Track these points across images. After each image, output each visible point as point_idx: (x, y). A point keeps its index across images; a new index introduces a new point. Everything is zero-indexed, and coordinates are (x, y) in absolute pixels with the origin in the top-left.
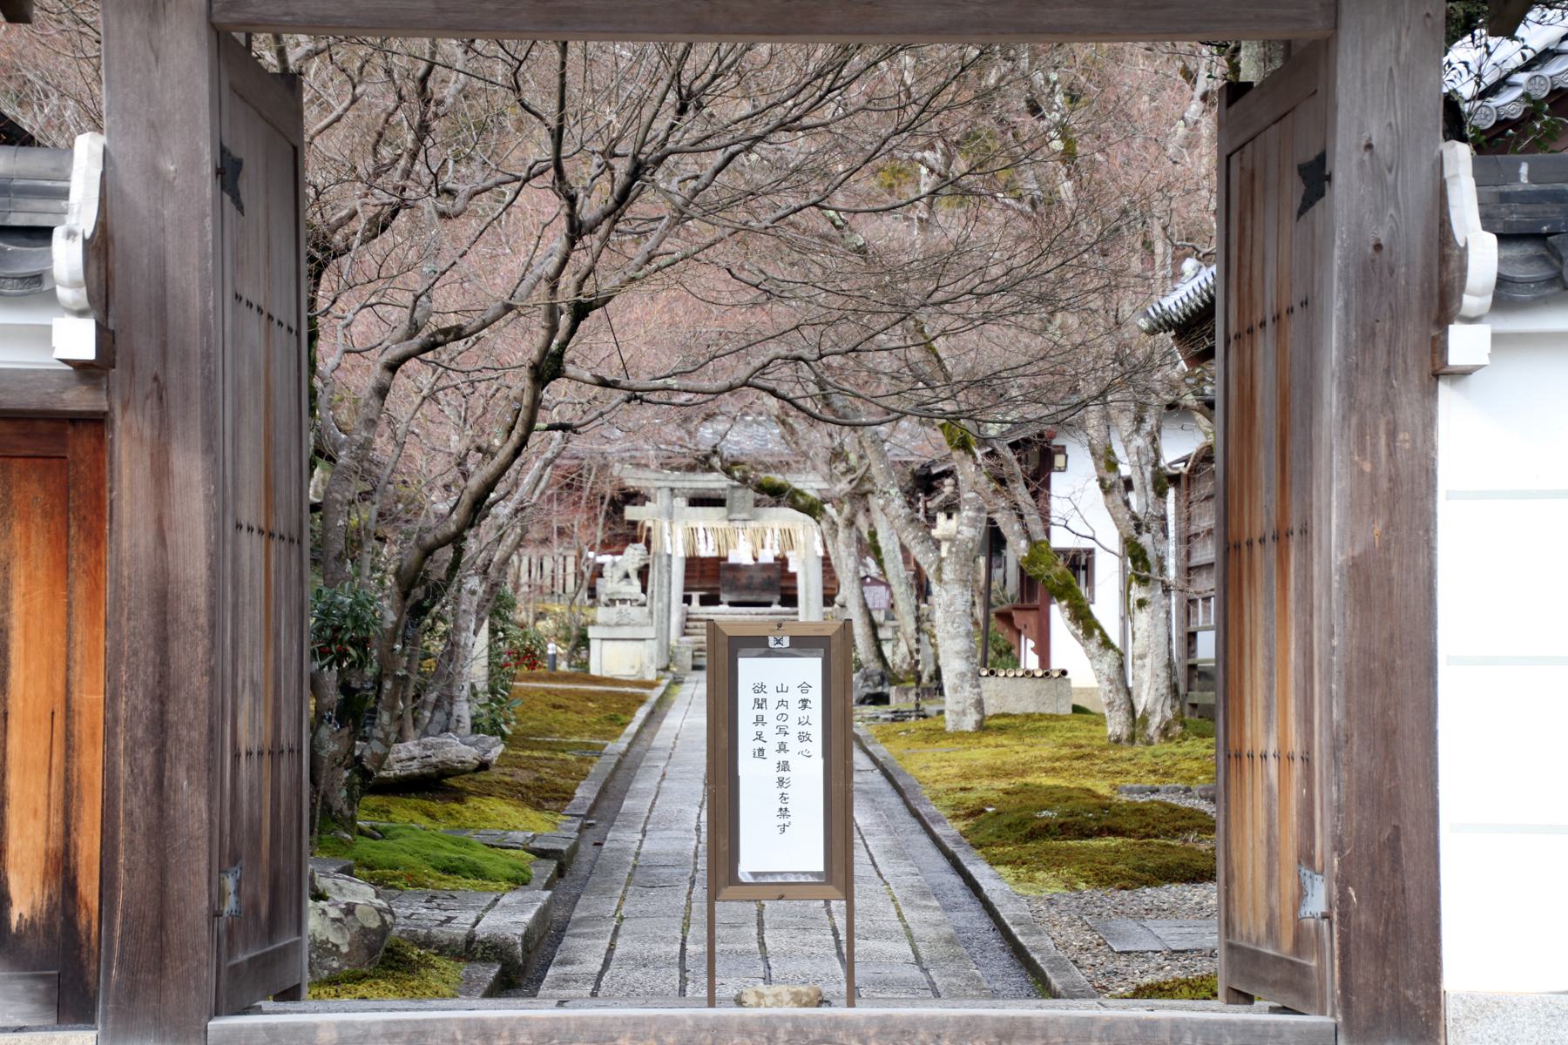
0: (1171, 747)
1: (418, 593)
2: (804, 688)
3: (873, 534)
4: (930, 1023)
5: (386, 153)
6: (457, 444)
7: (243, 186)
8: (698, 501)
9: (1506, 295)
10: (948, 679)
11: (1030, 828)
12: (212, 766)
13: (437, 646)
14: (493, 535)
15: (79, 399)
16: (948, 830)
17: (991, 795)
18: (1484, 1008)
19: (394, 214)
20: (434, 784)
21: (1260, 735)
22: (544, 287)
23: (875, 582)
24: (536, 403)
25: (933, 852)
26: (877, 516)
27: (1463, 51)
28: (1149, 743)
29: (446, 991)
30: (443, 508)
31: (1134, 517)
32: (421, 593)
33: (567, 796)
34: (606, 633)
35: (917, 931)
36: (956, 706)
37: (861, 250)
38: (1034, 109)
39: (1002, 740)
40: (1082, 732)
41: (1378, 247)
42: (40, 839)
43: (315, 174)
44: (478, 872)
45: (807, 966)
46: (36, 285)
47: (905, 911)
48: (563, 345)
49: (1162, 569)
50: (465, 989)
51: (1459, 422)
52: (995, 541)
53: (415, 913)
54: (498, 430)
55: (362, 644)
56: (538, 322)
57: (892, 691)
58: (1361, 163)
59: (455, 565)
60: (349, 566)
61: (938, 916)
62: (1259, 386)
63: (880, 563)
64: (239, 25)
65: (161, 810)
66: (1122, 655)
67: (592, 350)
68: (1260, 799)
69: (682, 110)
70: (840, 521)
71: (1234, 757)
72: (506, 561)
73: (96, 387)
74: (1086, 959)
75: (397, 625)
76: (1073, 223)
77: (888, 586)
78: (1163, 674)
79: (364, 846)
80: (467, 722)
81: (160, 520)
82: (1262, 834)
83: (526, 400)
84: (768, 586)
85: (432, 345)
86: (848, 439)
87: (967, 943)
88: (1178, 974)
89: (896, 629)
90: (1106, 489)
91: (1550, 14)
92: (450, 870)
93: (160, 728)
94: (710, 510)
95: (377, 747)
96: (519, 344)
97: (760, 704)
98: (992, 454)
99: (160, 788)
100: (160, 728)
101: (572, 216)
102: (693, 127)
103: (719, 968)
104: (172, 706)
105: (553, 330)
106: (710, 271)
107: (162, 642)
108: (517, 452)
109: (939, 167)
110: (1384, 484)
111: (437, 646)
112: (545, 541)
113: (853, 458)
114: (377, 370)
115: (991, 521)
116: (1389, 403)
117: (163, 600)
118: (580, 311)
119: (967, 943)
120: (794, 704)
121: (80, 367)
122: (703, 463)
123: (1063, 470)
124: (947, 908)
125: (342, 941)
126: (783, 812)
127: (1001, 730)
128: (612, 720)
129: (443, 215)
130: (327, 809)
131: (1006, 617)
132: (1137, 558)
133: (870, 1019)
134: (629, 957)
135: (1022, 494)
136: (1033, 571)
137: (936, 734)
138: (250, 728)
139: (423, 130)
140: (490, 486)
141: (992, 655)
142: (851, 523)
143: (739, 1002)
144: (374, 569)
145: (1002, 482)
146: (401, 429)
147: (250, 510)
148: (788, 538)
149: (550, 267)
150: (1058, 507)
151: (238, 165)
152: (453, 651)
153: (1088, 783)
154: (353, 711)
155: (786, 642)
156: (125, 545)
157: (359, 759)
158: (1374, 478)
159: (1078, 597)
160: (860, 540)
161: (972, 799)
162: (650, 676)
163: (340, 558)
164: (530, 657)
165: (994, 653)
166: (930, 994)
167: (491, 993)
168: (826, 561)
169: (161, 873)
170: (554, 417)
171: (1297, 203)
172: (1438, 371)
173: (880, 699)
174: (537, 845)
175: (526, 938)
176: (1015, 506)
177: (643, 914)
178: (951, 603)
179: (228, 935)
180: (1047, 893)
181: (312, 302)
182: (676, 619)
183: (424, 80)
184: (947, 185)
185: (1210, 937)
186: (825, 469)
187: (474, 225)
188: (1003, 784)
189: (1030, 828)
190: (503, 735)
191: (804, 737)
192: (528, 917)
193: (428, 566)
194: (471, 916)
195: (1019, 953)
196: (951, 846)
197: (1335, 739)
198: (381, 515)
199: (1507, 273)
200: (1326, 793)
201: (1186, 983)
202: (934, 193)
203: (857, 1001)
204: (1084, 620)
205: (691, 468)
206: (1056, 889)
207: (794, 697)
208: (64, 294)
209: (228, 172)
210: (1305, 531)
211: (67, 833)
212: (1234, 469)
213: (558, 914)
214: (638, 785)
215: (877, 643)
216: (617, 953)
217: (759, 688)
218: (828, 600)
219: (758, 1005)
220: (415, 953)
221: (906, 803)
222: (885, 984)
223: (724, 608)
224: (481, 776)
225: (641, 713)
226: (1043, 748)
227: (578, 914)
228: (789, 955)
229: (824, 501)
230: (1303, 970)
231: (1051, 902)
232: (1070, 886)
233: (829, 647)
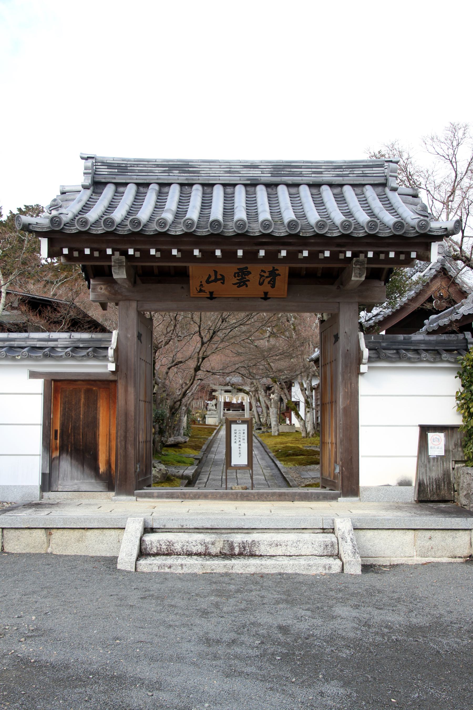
0: (313, 439)
1: (173, 410)
2: (244, 430)
3: (259, 398)
4: (266, 493)
5: (169, 330)
6: (181, 382)
7: (142, 339)
8: (226, 391)
9: (370, 360)
10: (272, 425)
11: (287, 454)
12: (135, 445)
13: (177, 419)
14: (187, 399)
15: (112, 378)
16: (272, 455)
17: (280, 448)
18: (367, 489)
19: (170, 341)
20: (176, 445)
21: (328, 440)
22: (197, 354)
23: (259, 407)
24: (195, 375)
25: (269, 459)
26: (259, 394)
27: (363, 314)
28: (310, 438)
29: (178, 485)
30: (178, 393)
31: (307, 396)
32: (174, 410)
33: (201, 448)
34: (209, 416)
35: (266, 474)
36: (274, 430)
37: (256, 346)
38: (288, 321)
39: (282, 437)
40: (297, 436)
41: (348, 350)
42: (105, 457)
43: (155, 334)
44: (184, 462)
45: (245, 481)
46: (105, 358)
47: (264, 471)
48: (200, 364)
49: (312, 405)
50: (181, 484)
51: (362, 382)
52: (281, 400)
53: (172, 470)
54: (188, 380)
55: (163, 420)
56: (196, 360)
57: (262, 427)
58: (344, 336)
59: (180, 405)
60: (161, 405)
61: (269, 471)
62: (327, 375)
63: (260, 403)
64: (142, 311)
65: (126, 453)
66: (305, 421)
67: (206, 365)
68: (328, 451)
69: (223, 322)
70: (252, 396)
71: (323, 443)
72: (190, 403)
73: (115, 375)
74: (297, 479)
75: (169, 416)
76: (295, 341)
77: (261, 407)
78: (312, 425)
79: (163, 457)
80: (182, 434)
81: (126, 399)
82: (328, 457)
83: (193, 375)
84: (239, 407)
85: (176, 364)
86: (254, 381)
87: (275, 476)
88: (313, 482)
89: (263, 415)
90: (302, 390)
91: (377, 308)
92: (179, 462)
93: (126, 437)
94: (228, 393)
95: (166, 439)
96: (192, 364)
97: (235, 433)
98: (280, 384)
99: (126, 449)
100: (126, 437)
101: (202, 341)
102: (225, 324)
103: (228, 481)
104: (128, 434)
105: (198, 362)
106: (227, 351)
107: (126, 422)
108: (192, 384)
109: (271, 331)
110: (350, 393)
111: (177, 419)
112: (198, 399)
113: (255, 384)
114: (166, 369)
115: (281, 396)
116: (350, 379)
117: (126, 414)
118: (203, 359)
119: (275, 476)
120: (242, 433)
121: (112, 372)
122: (227, 385)
123: (294, 386)
124: (271, 469)
125: (159, 475)
126: (240, 453)
127: (282, 435)
128: (210, 433)
129: (179, 341)
130: (157, 451)
131: (283, 414)
132: (307, 404)
133: (255, 492)
134: (212, 479)
135: (286, 391)
136: (288, 406)
137: (270, 436)
138: (142, 437)
139: (175, 326)
140: (186, 391)
141: (281, 420)
142: (255, 396)
143: (231, 489)
144: (166, 405)
145: (282, 389)
146: (171, 379)
147: (142, 398)
148: (243, 399)
149: (198, 351)
150: (293, 394)
151: (141, 335)
152: (180, 420)
153: (298, 445)
154: (161, 432)
155: (240, 422)
156: (120, 404)
157: (162, 441)
158: (348, 392)
159: (297, 410)
160: (256, 399)
161: (276, 448)
162: (217, 424)
163: (159, 404)
164: (194, 422)
165: (281, 420)
166: (268, 486)
167: (186, 486)
168: (250, 403)
169: (126, 464)
170: (199, 377)
171: (334, 342)
172: (359, 373)
173: (260, 429)
174: (195, 457)
175: (193, 475)
176: (285, 394)
177: (215, 471)
178: (273, 411)
179: (138, 475)
180: (290, 467)
181: (154, 358)
182: (222, 413)
183: (175, 317)
184: (273, 334)
185: (319, 475)
186: (250, 385)
187: (184, 343)
188: (282, 446)
189: (287, 454)
190: (189, 436)
191: (244, 439)
192: (193, 471)
193: (175, 405)
194: (183, 471)
195: (284, 478)
196: (272, 458)
197: (341, 440)
198: (167, 395)
199: (370, 356)
200: (339, 450)
201: (315, 484)
202: (269, 337)
203: (254, 489)
204: (298, 415)
205: (225, 385)
206: (292, 466)
207: (242, 432)
208: (110, 359)
209: (139, 336)
210: (336, 402)
211: (109, 456)
212: (323, 390)
213: (199, 470)
214: (214, 446)
215: (259, 418)
216: (210, 478)
217: (235, 430)
218: (251, 410)
219: (235, 490)
220: (172, 478)
221: (264, 449)
222: (259, 484)
223: (231, 411)
224: (185, 444)
225: (215, 431)
226: (290, 439)
227: (203, 470)
228: (242, 479)
229: (250, 391)
230: (335, 482)
231: (291, 468)
232: (294, 465)
233: (248, 422)
